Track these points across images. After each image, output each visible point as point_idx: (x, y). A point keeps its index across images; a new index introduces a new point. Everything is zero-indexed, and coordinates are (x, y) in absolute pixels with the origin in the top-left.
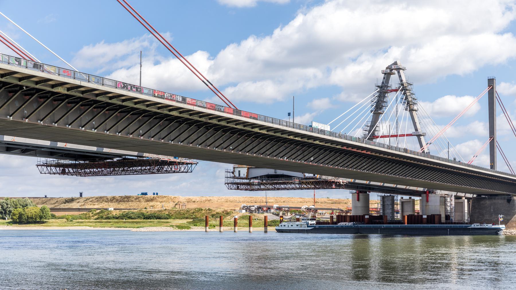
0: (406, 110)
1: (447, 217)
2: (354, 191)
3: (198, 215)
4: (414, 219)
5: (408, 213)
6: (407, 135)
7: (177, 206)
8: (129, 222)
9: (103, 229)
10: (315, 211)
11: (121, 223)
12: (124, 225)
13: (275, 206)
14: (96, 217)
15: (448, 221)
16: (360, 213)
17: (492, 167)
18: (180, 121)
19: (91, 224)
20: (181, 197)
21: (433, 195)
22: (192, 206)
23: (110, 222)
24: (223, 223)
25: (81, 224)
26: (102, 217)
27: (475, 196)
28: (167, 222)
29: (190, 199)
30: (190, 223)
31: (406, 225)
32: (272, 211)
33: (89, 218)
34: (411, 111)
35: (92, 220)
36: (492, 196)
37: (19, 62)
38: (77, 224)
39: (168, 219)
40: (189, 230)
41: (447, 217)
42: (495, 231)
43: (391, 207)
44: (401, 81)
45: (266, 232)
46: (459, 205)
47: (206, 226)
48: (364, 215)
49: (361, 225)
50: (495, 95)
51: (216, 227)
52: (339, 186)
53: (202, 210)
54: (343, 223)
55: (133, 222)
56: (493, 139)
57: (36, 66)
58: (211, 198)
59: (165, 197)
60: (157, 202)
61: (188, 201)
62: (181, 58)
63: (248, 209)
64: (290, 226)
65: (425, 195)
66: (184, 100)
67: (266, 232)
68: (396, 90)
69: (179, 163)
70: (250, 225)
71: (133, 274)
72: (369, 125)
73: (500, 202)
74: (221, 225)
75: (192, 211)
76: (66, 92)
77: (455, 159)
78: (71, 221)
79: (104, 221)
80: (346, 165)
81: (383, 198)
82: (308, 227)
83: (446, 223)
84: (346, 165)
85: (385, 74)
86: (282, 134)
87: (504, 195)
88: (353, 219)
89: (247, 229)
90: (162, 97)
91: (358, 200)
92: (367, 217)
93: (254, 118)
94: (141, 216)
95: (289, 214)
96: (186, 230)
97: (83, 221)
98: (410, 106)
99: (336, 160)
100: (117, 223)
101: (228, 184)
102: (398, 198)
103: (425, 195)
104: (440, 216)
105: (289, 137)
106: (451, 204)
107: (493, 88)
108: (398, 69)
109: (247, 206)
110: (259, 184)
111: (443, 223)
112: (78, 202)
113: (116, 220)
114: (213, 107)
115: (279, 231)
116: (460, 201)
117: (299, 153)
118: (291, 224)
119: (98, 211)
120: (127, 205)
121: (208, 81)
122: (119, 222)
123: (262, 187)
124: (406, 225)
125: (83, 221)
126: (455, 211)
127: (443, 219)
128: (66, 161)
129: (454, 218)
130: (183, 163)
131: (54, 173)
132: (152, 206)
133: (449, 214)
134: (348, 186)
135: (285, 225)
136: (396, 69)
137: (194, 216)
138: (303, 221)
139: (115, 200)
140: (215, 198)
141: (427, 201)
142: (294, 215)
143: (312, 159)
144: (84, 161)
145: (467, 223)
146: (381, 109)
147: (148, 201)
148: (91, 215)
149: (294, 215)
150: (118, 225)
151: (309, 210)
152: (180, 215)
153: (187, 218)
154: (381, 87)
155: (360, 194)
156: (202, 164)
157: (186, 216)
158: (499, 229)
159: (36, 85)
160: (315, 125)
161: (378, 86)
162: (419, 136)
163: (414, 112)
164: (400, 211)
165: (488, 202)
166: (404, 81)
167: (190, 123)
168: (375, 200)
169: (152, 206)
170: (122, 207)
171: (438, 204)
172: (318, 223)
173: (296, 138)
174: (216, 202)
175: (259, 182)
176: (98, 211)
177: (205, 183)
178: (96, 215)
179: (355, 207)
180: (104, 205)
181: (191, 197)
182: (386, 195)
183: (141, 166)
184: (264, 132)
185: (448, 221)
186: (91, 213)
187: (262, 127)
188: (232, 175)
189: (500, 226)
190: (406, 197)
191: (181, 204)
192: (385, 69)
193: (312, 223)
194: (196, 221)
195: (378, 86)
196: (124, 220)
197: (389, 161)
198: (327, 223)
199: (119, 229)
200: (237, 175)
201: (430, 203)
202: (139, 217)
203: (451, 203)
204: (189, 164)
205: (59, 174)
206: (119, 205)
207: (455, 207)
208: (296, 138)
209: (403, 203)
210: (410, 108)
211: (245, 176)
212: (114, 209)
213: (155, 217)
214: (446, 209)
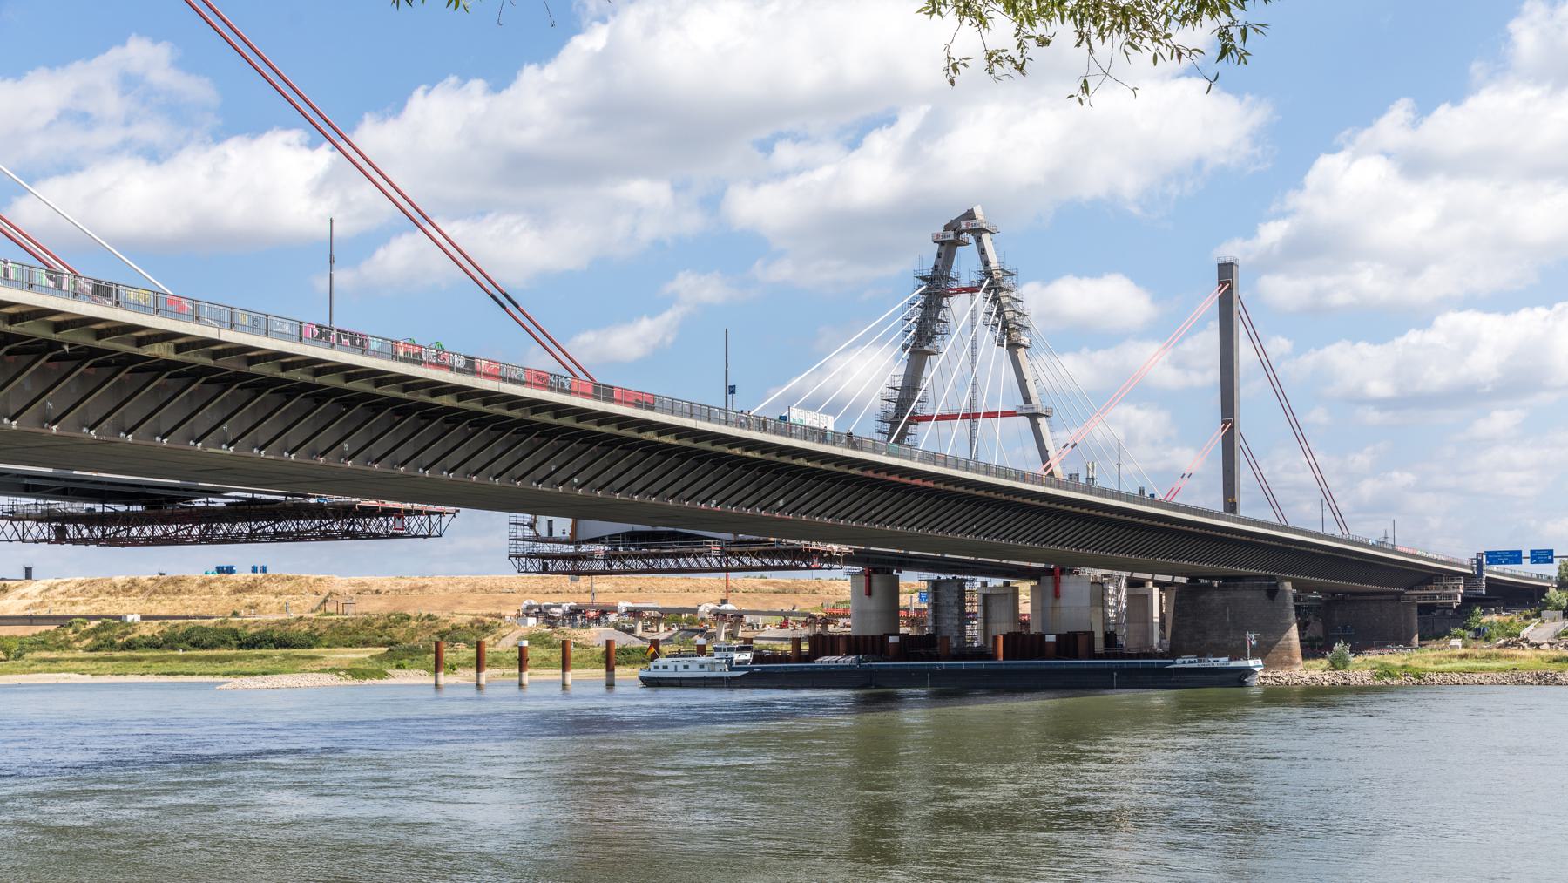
0: (1000, 344)
1: (1110, 638)
2: (858, 569)
3: (399, 633)
4: (1022, 643)
5: (1002, 628)
6: (1004, 414)
7: (330, 608)
8: (199, 659)
9: (121, 679)
10: (738, 618)
11: (176, 663)
12: (183, 667)
13: (623, 605)
14: (86, 642)
15: (1112, 650)
16: (873, 630)
17: (1231, 506)
18: (453, 417)
19: (83, 666)
20: (336, 578)
21: (1073, 578)
22: (374, 607)
23: (140, 659)
24: (488, 659)
25: (53, 666)
26: (112, 645)
27: (1183, 580)
28: (312, 658)
29: (363, 584)
30: (379, 658)
31: (1001, 661)
32: (612, 617)
33: (67, 645)
34: (1014, 347)
35: (80, 654)
36: (1230, 581)
37: (55, 280)
38: (39, 667)
39: (310, 646)
40: (384, 682)
41: (1110, 638)
42: (1236, 676)
43: (956, 611)
44: (987, 263)
45: (610, 685)
46: (1139, 603)
47: (437, 670)
48: (887, 636)
49: (878, 664)
51: (459, 670)
52: (831, 559)
53: (408, 618)
54: (827, 659)
55: (209, 659)
56: (1232, 427)
57: (102, 291)
58: (427, 581)
59: (289, 579)
60: (266, 593)
61: (358, 589)
62: (427, 227)
63: (543, 614)
64: (680, 668)
65: (1049, 577)
66: (470, 367)
67: (610, 685)
68: (972, 290)
69: (408, 512)
70: (565, 666)
71: (325, 828)
72: (899, 384)
73: (1249, 597)
74: (479, 664)
75: (381, 622)
76: (173, 356)
77: (1141, 491)
78: (19, 656)
79: (118, 654)
80: (866, 517)
81: (935, 585)
82: (731, 669)
83: (1107, 656)
84: (866, 517)
85: (942, 243)
86: (714, 444)
87: (1258, 577)
88: (853, 644)
89: (555, 674)
90: (416, 360)
91: (869, 593)
92: (893, 640)
93: (638, 405)
94: (229, 638)
95: (662, 628)
96: (376, 681)
97: (54, 655)
98: (1010, 333)
99: (840, 505)
100: (163, 660)
101: (518, 557)
102: (976, 583)
103: (1049, 579)
104: (1091, 634)
105: (732, 451)
106: (1118, 602)
107: (1230, 289)
108: (978, 232)
109: (539, 607)
110: (607, 557)
111: (1100, 656)
112: (23, 596)
113: (157, 653)
114: (543, 381)
115: (650, 683)
116: (1140, 591)
117: (748, 490)
118: (684, 661)
119: (94, 624)
120: (177, 604)
121: (506, 295)
122: (170, 658)
123: (616, 565)
124: (1001, 661)
125: (54, 655)
126: (1128, 621)
127: (1099, 645)
128: (76, 505)
129: (1126, 639)
130: (419, 513)
131: (36, 541)
132: (251, 607)
133: (1112, 628)
134: (848, 560)
135: (667, 666)
136: (969, 231)
137: (387, 638)
138: (717, 655)
139: (136, 590)
140: (438, 582)
141: (1057, 595)
142: (675, 629)
143: (781, 503)
144: (128, 504)
145: (1161, 656)
146: (930, 340)
147: (239, 592)
148: (72, 636)
149: (675, 629)
150: (166, 668)
151: (720, 616)
152: (347, 635)
153: (366, 644)
154: (930, 280)
155: (875, 577)
156: (468, 517)
157: (363, 637)
158: (1248, 671)
159: (98, 339)
160: (797, 415)
161: (924, 278)
162: (1034, 417)
163: (1021, 351)
164: (980, 615)
165: (1218, 598)
166: (994, 264)
167: (478, 421)
168: (913, 588)
169: (251, 607)
170: (162, 611)
171: (1086, 603)
172: (759, 658)
173: (749, 454)
174: (442, 594)
175: (606, 553)
176: (94, 624)
177: (468, 559)
178: (87, 634)
179: (861, 613)
180: (109, 606)
181: (367, 579)
182: (943, 577)
183: (298, 517)
184: (669, 439)
185: (1112, 650)
186: (70, 631)
187: (664, 429)
188: (529, 532)
189: (1251, 663)
190: (996, 582)
191: (341, 601)
193: (743, 658)
194: (398, 653)
195: (924, 278)
196: (181, 653)
197: (979, 501)
198: (784, 658)
199: (171, 679)
200: (544, 533)
201: (1063, 602)
202: (223, 642)
203: (1118, 597)
204: (434, 513)
205: (48, 541)
206: (153, 605)
207: (1127, 609)
208: (749, 454)
209: (987, 599)
210: (1009, 339)
211: (567, 535)
212: (143, 618)
213: (272, 641)
214: (1105, 614)
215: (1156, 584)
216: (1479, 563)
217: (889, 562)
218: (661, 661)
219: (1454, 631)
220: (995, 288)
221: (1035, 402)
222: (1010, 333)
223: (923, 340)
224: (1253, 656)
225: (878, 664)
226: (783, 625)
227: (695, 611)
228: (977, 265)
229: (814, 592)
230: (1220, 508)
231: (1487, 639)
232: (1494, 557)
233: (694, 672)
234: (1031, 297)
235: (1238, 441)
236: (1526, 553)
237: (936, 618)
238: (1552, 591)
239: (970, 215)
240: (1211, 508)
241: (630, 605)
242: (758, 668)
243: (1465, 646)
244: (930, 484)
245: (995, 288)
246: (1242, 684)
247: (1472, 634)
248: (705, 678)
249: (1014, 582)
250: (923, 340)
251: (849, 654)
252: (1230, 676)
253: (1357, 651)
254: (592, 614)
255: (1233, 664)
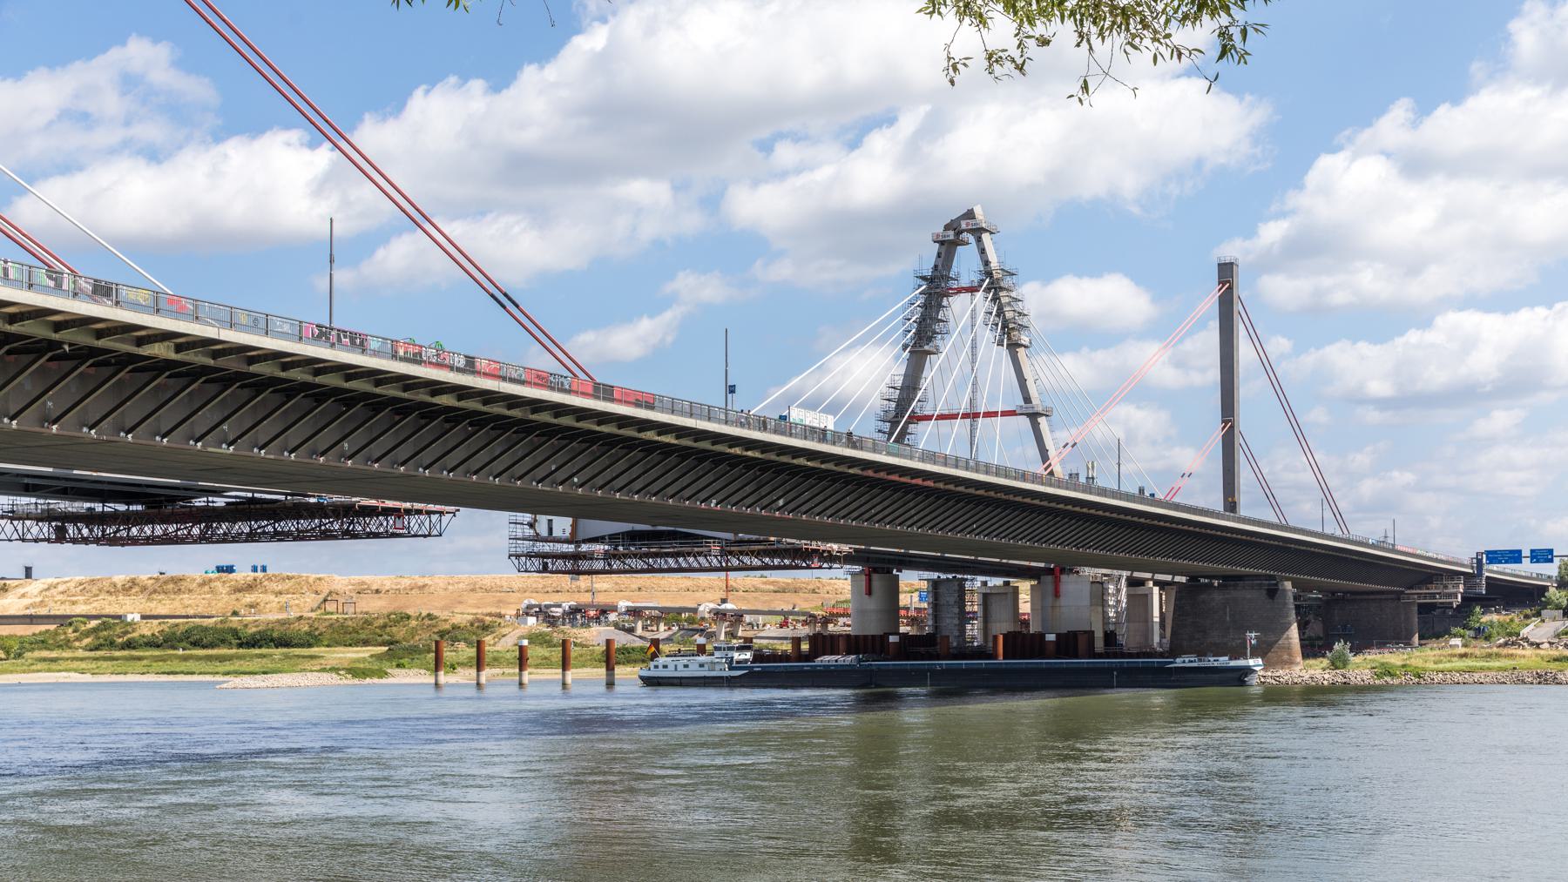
0: (1000, 344)
1: (1110, 637)
2: (858, 568)
3: (399, 632)
4: (1022, 642)
5: (1002, 627)
6: (1004, 414)
7: (330, 607)
8: (199, 658)
9: (121, 678)
10: (738, 617)
11: (176, 662)
12: (183, 666)
13: (623, 605)
14: (86, 641)
15: (1112, 649)
16: (873, 629)
17: (1231, 506)
18: (453, 417)
19: (83, 665)
20: (336, 577)
21: (1073, 577)
22: (374, 606)
23: (140, 659)
24: (488, 658)
25: (53, 666)
26: (112, 644)
27: (1183, 579)
28: (312, 657)
29: (363, 583)
30: (379, 657)
31: (1001, 660)
32: (612, 617)
33: (67, 644)
34: (1014, 346)
35: (80, 653)
36: (1230, 580)
37: (55, 280)
38: (39, 666)
39: (310, 646)
40: (384, 681)
41: (1110, 637)
42: (1236, 675)
43: (956, 610)
44: (987, 263)
45: (610, 684)
46: (1139, 602)
47: (437, 669)
48: (887, 635)
49: (878, 663)
51: (459, 669)
52: (831, 558)
53: (408, 617)
54: (827, 658)
55: (209, 658)
56: (1232, 427)
57: (102, 290)
58: (427, 581)
59: (289, 578)
60: (266, 592)
61: (358, 588)
62: (427, 226)
63: (543, 613)
64: (680, 667)
65: (1049, 577)
66: (470, 366)
67: (610, 684)
68: (972, 290)
69: (408, 512)
70: (565, 665)
71: (325, 828)
72: (899, 384)
73: (1249, 596)
74: (479, 663)
75: (381, 622)
76: (173, 356)
77: (1141, 491)
78: (19, 655)
79: (118, 654)
80: (866, 516)
81: (935, 584)
82: (731, 668)
83: (1107, 655)
84: (866, 516)
85: (942, 243)
86: (714, 444)
87: (1258, 577)
88: (853, 644)
89: (555, 674)
90: (416, 359)
91: (869, 592)
92: (893, 639)
93: (638, 404)
94: (229, 637)
95: (662, 627)
96: (376, 680)
97: (54, 654)
98: (1010, 333)
99: (840, 505)
100: (163, 659)
101: (518, 556)
102: (976, 583)
103: (1049, 579)
104: (1091, 634)
105: (732, 451)
106: (1118, 602)
107: (1230, 288)
108: (978, 232)
109: (539, 606)
110: (607, 556)
111: (1100, 656)
112: (23, 596)
113: (157, 653)
114: (543, 380)
115: (650, 682)
116: (1140, 590)
117: (748, 489)
118: (684, 660)
119: (94, 623)
120: (177, 604)
121: (506, 295)
122: (170, 657)
123: (616, 565)
124: (1001, 660)
125: (54, 654)
126: (1128, 620)
127: (1099, 645)
128: (76, 504)
129: (1126, 638)
130: (419, 512)
131: (36, 540)
132: (251, 606)
133: (1112, 628)
134: (848, 559)
135: (667, 665)
136: (969, 231)
137: (387, 637)
138: (717, 654)
139: (136, 589)
140: (438, 581)
141: (1057, 594)
142: (675, 628)
143: (781, 502)
144: (128, 504)
145: (1161, 655)
146: (930, 339)
147: (239, 591)
148: (72, 636)
149: (675, 628)
150: (166, 667)
151: (720, 615)
152: (347, 634)
153: (366, 643)
154: (930, 280)
155: (875, 577)
156: (468, 516)
157: (363, 636)
158: (1248, 671)
159: (98, 338)
160: (797, 415)
161: (924, 278)
162: (1034, 417)
163: (1021, 351)
164: (980, 614)
165: (1218, 597)
166: (994, 264)
167: (478, 421)
168: (913, 587)
169: (251, 606)
170: (162, 610)
171: (1086, 602)
172: (759, 657)
173: (749, 453)
174: (442, 593)
175: (606, 552)
176: (94, 623)
177: (468, 559)
178: (87, 634)
179: (861, 612)
180: (109, 606)
181: (367, 578)
182: (943, 576)
183: (298, 517)
184: (669, 439)
185: (1112, 649)
186: (70, 630)
187: (664, 428)
188: (529, 532)
189: (1251, 662)
190: (996, 582)
191: (341, 600)
193: (743, 657)
194: (398, 653)
195: (924, 278)
196: (181, 652)
197: (979, 500)
198: (784, 657)
199: (171, 678)
200: (544, 532)
201: (1063, 601)
202: (223, 641)
203: (1118, 596)
204: (434, 512)
205: (48, 540)
206: (153, 605)
207: (1127, 609)
208: (749, 453)
209: (987, 598)
210: (1009, 338)
211: (567, 534)
212: (143, 617)
213: (272, 640)
214: (1105, 613)
215: (1156, 583)
216: (1479, 562)
217: (889, 561)
218: (661, 660)
219: (1454, 630)
220: (995, 288)
221: (1035, 401)
222: (1010, 333)
223: (923, 340)
224: (1253, 656)
225: (878, 663)
226: (783, 625)
227: (695, 610)
228: (977, 265)
229: (814, 591)
230: (1220, 508)
231: (1487, 638)
232: (1494, 556)
233: (694, 671)
234: (1031, 297)
235: (1238, 440)
236: (1526, 553)
237: (936, 617)
238: (1552, 590)
239: (970, 215)
240: (1211, 507)
241: (630, 604)
242: (758, 667)
243: (1465, 646)
244: (930, 483)
245: (995, 288)
246: (1242, 683)
247: (1472, 633)
248: (705, 677)
249: (1014, 582)
250: (923, 340)
251: (849, 653)
252: (1230, 675)
253: (1357, 650)
254: (592, 613)
255: (1233, 663)
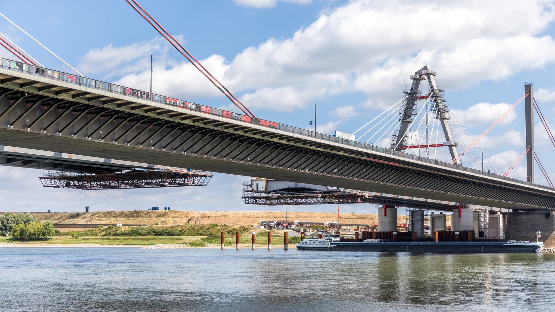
0: (437, 118)
1: (481, 234)
2: (381, 206)
3: (213, 231)
4: (446, 235)
5: (439, 229)
6: (438, 145)
7: (191, 222)
8: (139, 239)
9: (111, 246)
10: (339, 227)
11: (131, 240)
12: (133, 242)
13: (296, 221)
14: (103, 233)
15: (482, 238)
16: (387, 229)
17: (530, 179)
18: (194, 130)
19: (98, 241)
20: (195, 212)
21: (466, 209)
22: (207, 222)
23: (118, 239)
24: (240, 240)
25: (88, 241)
26: (110, 234)
27: (511, 211)
28: (180, 239)
29: (204, 214)
30: (204, 240)
31: (437, 242)
32: (293, 227)
33: (96, 234)
34: (442, 119)
35: (99, 237)
36: (529, 211)
37: (20, 66)
38: (82, 241)
39: (180, 235)
40: (203, 248)
41: (481, 234)
42: (532, 248)
43: (420, 223)
44: (432, 87)
45: (286, 249)
46: (494, 221)
47: (222, 243)
48: (392, 231)
49: (388, 242)
50: (533, 102)
51: (232, 244)
52: (364, 200)
53: (217, 226)
54: (369, 240)
55: (143, 239)
56: (531, 150)
57: (39, 71)
58: (227, 213)
59: (177, 212)
60: (169, 217)
61: (202, 216)
62: (195, 63)
63: (266, 225)
64: (312, 243)
65: (457, 209)
66: (198, 108)
67: (286, 249)
68: (426, 97)
69: (193, 176)
70: (269, 242)
71: (143, 295)
72: (397, 134)
73: (538, 217)
74: (237, 242)
75: (207, 227)
76: (71, 99)
77: (489, 171)
78: (77, 238)
79: (112, 237)
80: (372, 178)
81: (412, 213)
82: (331, 244)
83: (480, 240)
84: (372, 178)
85: (414, 79)
86: (303, 144)
87: (542, 209)
88: (379, 235)
89: (266, 246)
90: (174, 105)
91: (385, 215)
92: (394, 233)
93: (273, 127)
94: (152, 232)
95: (311, 230)
96: (200, 247)
97: (89, 237)
98: (441, 114)
99: (361, 172)
100: (126, 239)
101: (245, 198)
102: (428, 213)
103: (457, 210)
104: (473, 232)
105: (311, 148)
106: (485, 220)
107: (530, 95)
108: (428, 75)
109: (266, 222)
110: (279, 198)
111: (477, 240)
112: (84, 218)
113: (125, 237)
114: (229, 115)
115: (300, 248)
116: (495, 216)
117: (322, 164)
118: (313, 241)
119: (106, 227)
120: (137, 221)
121: (223, 87)
122: (129, 239)
123: (282, 201)
124: (437, 242)
125: (89, 237)
126: (489, 227)
127: (477, 236)
128: (71, 173)
129: (488, 234)
130: (197, 176)
131: (58, 187)
132: (164, 222)
133: (482, 230)
134: (374, 200)
135: (307, 242)
136: (426, 74)
137: (208, 233)
138: (326, 238)
139: (123, 215)
140: (231, 213)
141: (460, 216)
142: (316, 231)
143: (336, 171)
144: (91, 173)
145: (502, 240)
146: (409, 117)
147: (160, 216)
148: (98, 231)
149: (316, 231)
150: (127, 242)
151: (332, 226)
152: (194, 232)
153: (201, 235)
154: (409, 94)
155: (388, 209)
156: (218, 177)
157: (200, 232)
158: (537, 247)
159: (39, 91)
160: (339, 134)
161: (407, 93)
162: (450, 146)
163: (445, 121)
164: (430, 227)
165: (525, 217)
166: (435, 87)
167: (204, 132)
168: (403, 215)
169: (164, 222)
170: (131, 223)
171: (471, 219)
172: (342, 240)
173: (319, 149)
174: (232, 218)
175: (278, 196)
176: (106, 227)
177: (221, 196)
178: (103, 231)
179: (382, 223)
180: (112, 221)
181: (205, 212)
182: (415, 209)
183: (152, 178)
184: (284, 142)
185: (482, 238)
186: (98, 229)
187: (281, 137)
188: (249, 188)
189: (538, 243)
190: (437, 212)
191: (195, 220)
192: (414, 74)
193: (336, 239)
194: (210, 238)
195: (407, 93)
196: (134, 237)
197: (419, 173)
198: (352, 240)
199: (128, 246)
200: (255, 189)
201: (462, 219)
202: (149, 233)
203: (485, 218)
204: (204, 176)
205: (64, 187)
206: (128, 221)
207: (489, 223)
208: (319, 149)
209: (433, 219)
210: (441, 116)
211: (264, 189)
212: (123, 225)
213: (167, 233)
214: (479, 225)
